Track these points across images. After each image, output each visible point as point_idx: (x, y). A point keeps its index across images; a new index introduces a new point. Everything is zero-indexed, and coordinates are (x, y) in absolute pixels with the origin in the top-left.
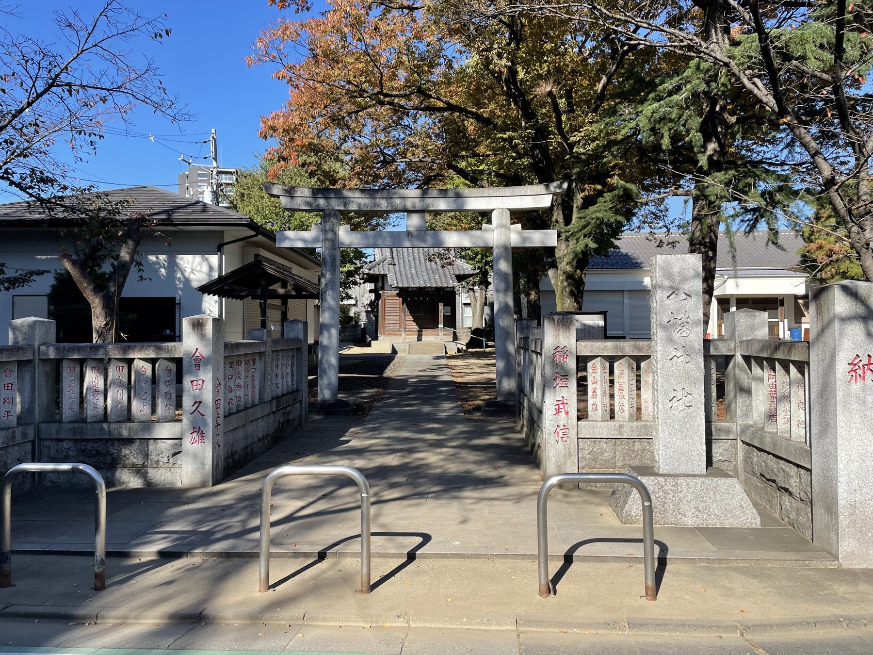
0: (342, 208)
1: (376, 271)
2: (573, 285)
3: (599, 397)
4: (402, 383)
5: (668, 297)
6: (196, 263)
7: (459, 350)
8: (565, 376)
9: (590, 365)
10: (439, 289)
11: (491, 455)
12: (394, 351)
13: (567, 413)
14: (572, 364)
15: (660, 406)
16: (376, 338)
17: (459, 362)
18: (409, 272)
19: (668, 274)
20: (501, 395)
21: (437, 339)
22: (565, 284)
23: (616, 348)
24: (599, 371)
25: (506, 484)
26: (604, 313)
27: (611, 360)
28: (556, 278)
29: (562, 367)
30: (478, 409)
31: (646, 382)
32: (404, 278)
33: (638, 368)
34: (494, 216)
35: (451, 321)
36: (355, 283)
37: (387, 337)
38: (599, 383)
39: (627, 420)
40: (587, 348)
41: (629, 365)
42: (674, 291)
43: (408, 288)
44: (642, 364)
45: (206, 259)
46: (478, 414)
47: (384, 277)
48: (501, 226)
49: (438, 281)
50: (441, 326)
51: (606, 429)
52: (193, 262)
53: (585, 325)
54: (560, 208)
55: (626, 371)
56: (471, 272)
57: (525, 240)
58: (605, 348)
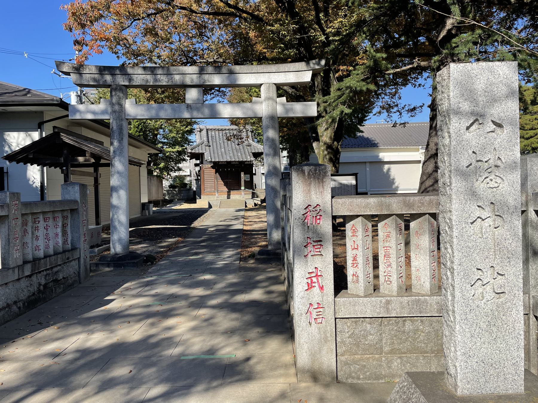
0: (127, 84)
1: (196, 151)
2: (331, 153)
3: (360, 266)
4: (203, 231)
5: (468, 128)
6: (21, 139)
7: (256, 205)
8: (319, 241)
9: (349, 226)
11: (248, 318)
13: (322, 288)
14: (326, 226)
15: (457, 294)
17: (254, 213)
18: (219, 151)
19: (468, 93)
20: (271, 244)
21: (241, 196)
22: (326, 152)
23: (381, 205)
24: (360, 233)
25: (249, 377)
26: (355, 175)
27: (375, 219)
28: (319, 148)
29: (315, 231)
30: (252, 256)
31: (418, 246)
32: (216, 155)
33: (407, 228)
35: (250, 185)
36: (184, 160)
37: (205, 197)
38: (360, 249)
39: (395, 294)
40: (346, 206)
41: (398, 226)
42: (478, 118)
43: (219, 162)
44: (412, 224)
45: (29, 135)
46: (252, 261)
47: (202, 154)
48: (268, 99)
49: (240, 157)
50: (243, 188)
51: (368, 307)
52: (18, 138)
53: (341, 184)
54: (321, 93)
55: (393, 234)
58: (367, 206)
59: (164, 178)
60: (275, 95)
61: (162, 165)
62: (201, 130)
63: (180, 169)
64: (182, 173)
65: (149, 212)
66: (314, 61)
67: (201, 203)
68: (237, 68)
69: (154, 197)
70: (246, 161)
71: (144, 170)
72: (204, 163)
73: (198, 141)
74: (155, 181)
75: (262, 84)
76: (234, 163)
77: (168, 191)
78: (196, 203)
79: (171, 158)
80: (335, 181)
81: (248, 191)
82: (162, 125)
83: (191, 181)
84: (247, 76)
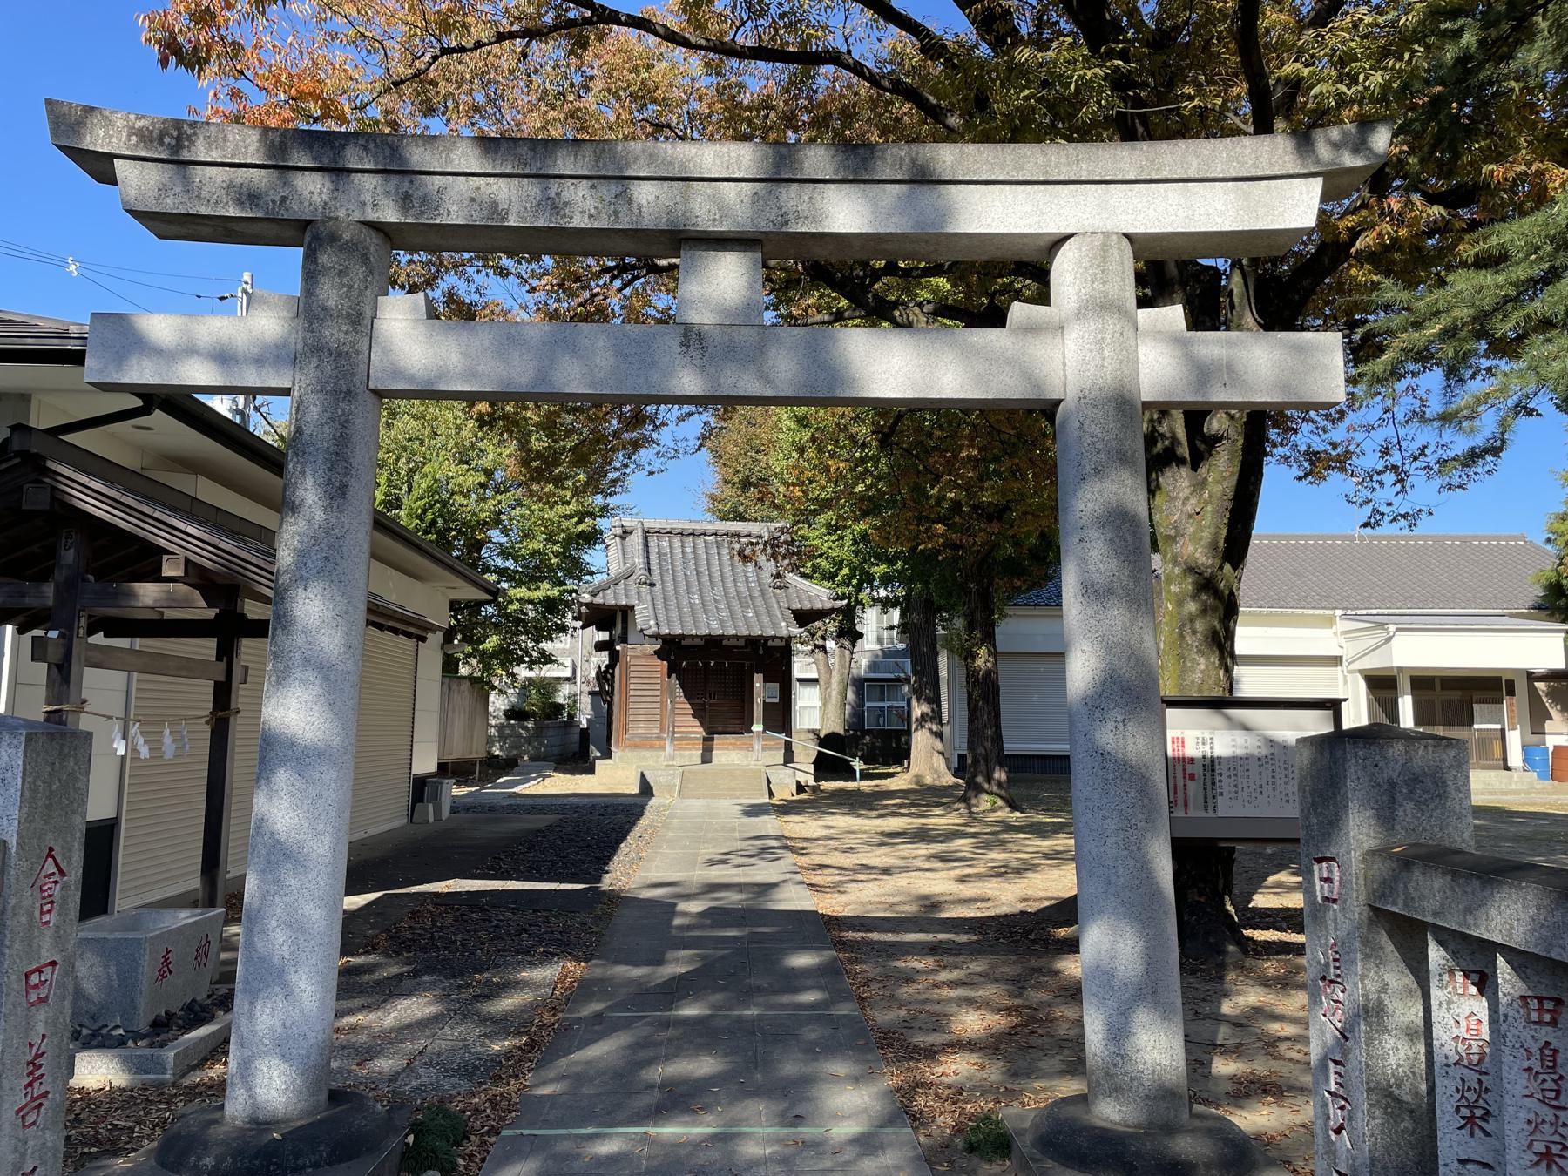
1: (609, 599)
4: (653, 920)
10: (753, 642)
12: (646, 790)
16: (607, 754)
21: (749, 759)
22: (1192, 607)
32: (674, 614)
34: (1066, 272)
35: (780, 717)
36: (563, 629)
43: (682, 637)
47: (627, 611)
48: (1103, 306)
50: (757, 727)
53: (1271, 742)
56: (829, 605)
57: (1203, 373)
59: (494, 688)
60: (1130, 292)
61: (492, 642)
62: (625, 534)
63: (547, 659)
64: (549, 672)
65: (437, 811)
66: (1335, 133)
67: (612, 776)
68: (947, 157)
69: (457, 753)
70: (773, 638)
71: (431, 655)
72: (631, 638)
73: (616, 568)
74: (463, 695)
75: (1064, 239)
76: (733, 642)
77: (500, 727)
78: (591, 770)
79: (518, 621)
80: (1246, 728)
81: (773, 739)
82: (500, 513)
83: (573, 698)
84: (993, 197)
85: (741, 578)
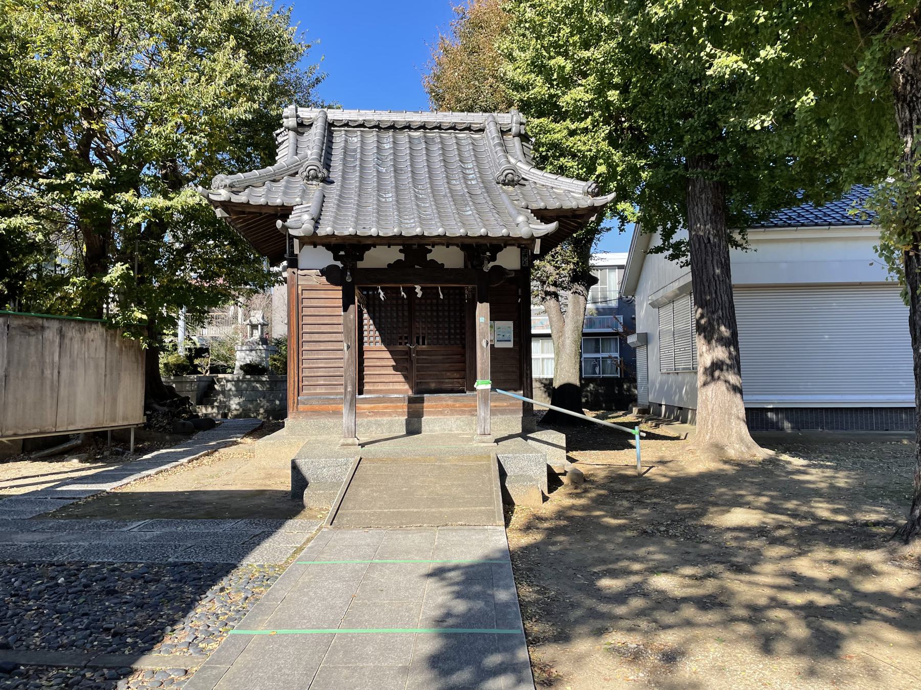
35: (514, 368)
37: (302, 422)
50: (483, 384)
62: (302, 127)
85: (457, 175)
